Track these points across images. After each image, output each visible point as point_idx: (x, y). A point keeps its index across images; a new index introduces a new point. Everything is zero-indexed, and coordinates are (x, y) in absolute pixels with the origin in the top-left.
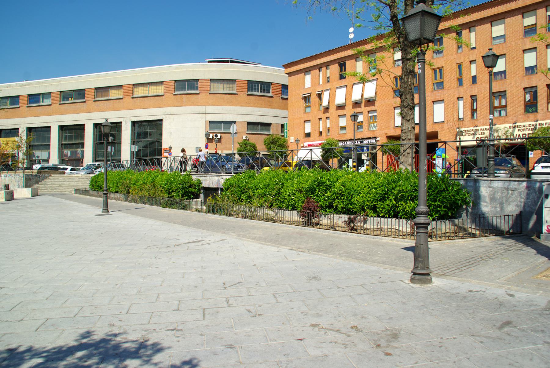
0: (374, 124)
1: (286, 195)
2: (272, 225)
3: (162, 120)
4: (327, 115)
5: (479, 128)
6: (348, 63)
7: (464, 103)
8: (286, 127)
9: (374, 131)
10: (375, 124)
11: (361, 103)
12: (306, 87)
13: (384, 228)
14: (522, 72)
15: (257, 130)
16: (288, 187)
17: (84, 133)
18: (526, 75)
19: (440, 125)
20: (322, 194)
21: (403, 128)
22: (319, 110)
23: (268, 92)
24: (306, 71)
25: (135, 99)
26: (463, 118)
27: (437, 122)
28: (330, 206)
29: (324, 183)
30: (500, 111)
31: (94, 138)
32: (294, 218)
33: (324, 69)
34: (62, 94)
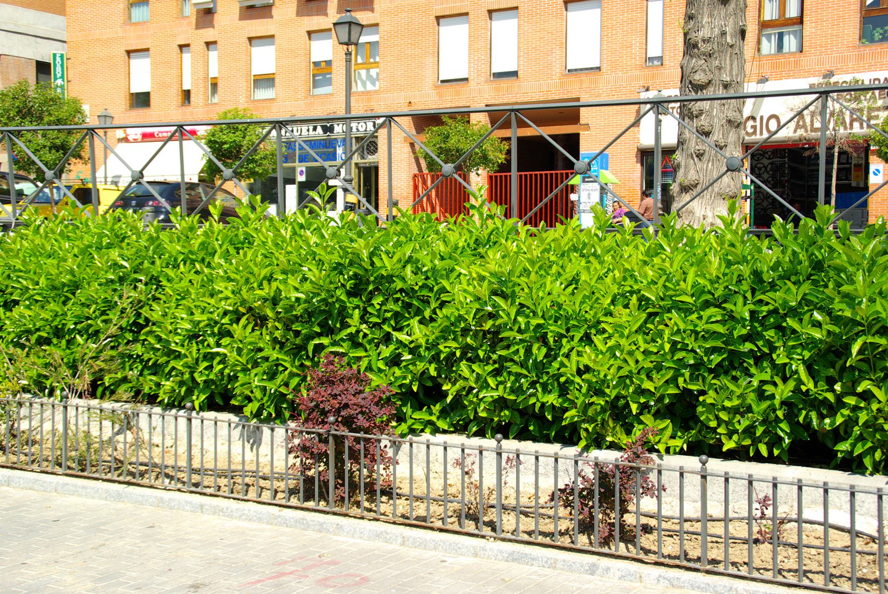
0: (368, 70)
1: (175, 332)
2: (119, 497)
4: (209, 34)
8: (59, 69)
9: (368, 93)
10: (373, 72)
13: (799, 520)
16: (184, 295)
19: (585, 78)
20: (378, 334)
21: (701, 34)
22: (181, 16)
26: (660, 58)
27: (576, 70)
29: (390, 279)
30: (781, 36)
32: (223, 449)
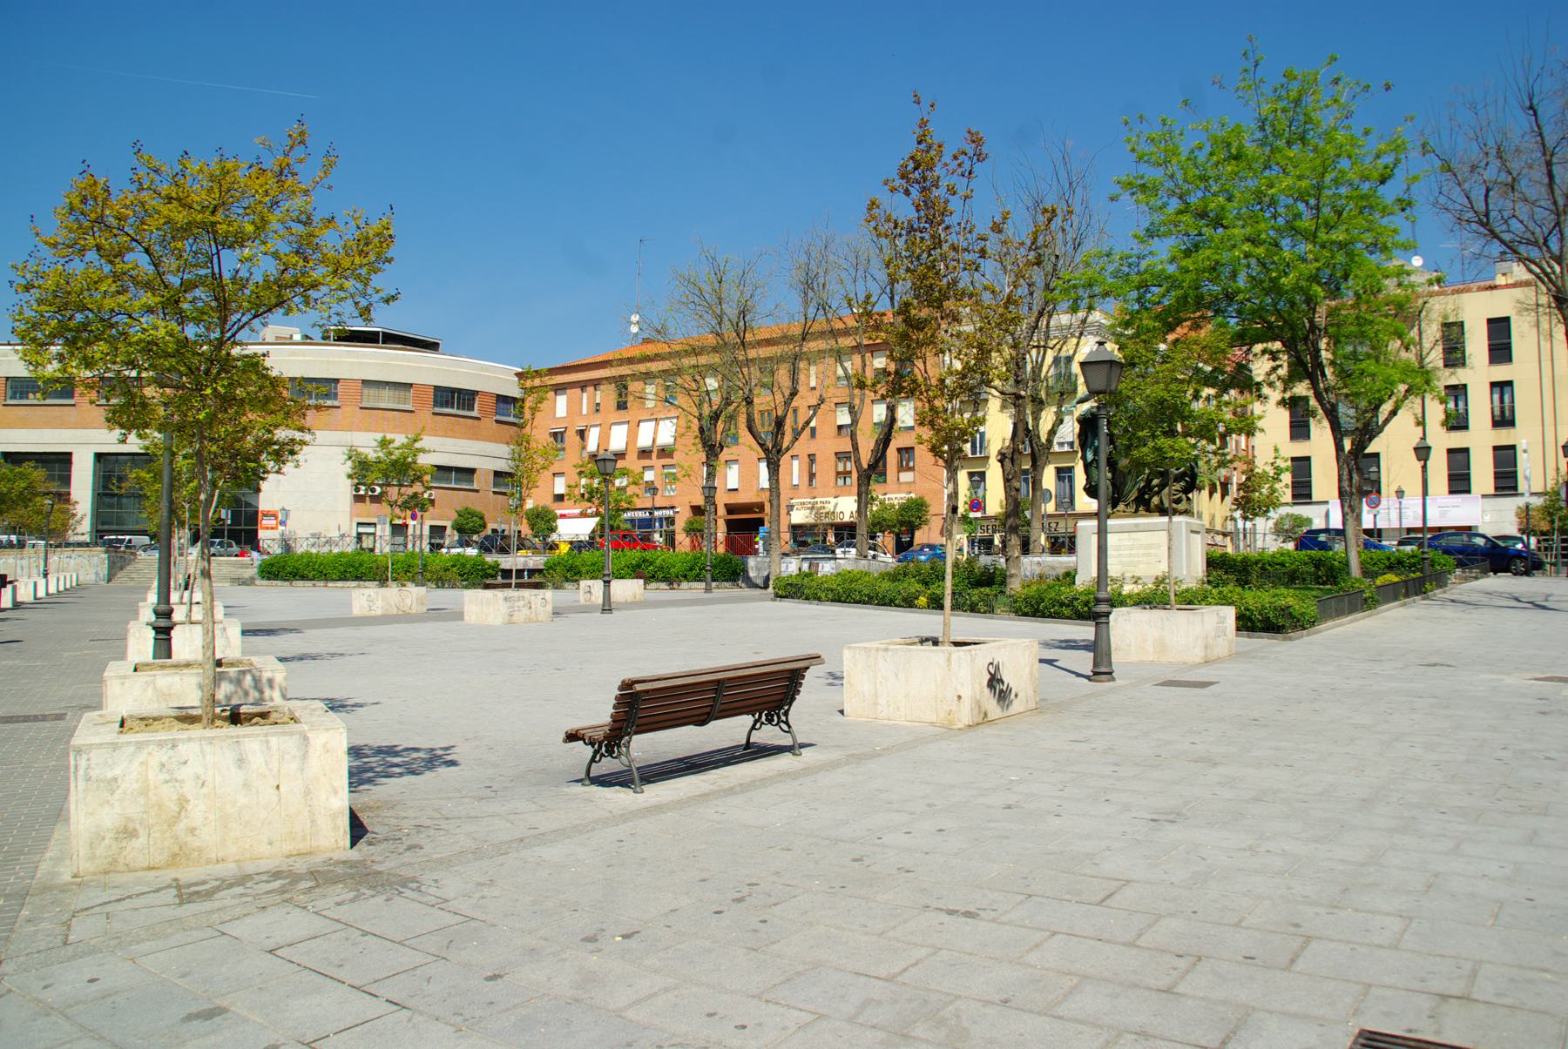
5: (818, 500)
7: (800, 463)
10: (673, 487)
12: (558, 416)
15: (449, 480)
17: (70, 471)
23: (471, 408)
28: (653, 577)
31: (94, 483)
33: (590, 389)
34: (9, 383)
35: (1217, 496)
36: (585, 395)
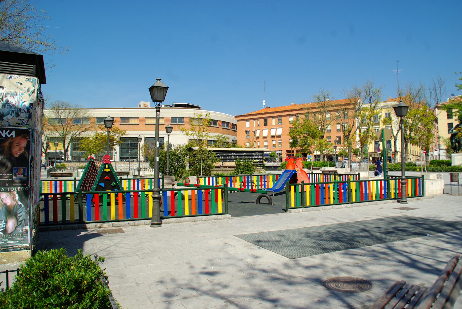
3: (163, 137)
4: (258, 140)
6: (268, 119)
11: (274, 136)
14: (336, 131)
18: (337, 132)
23: (216, 125)
24: (247, 120)
25: (147, 125)
35: (418, 147)
36: (255, 122)
